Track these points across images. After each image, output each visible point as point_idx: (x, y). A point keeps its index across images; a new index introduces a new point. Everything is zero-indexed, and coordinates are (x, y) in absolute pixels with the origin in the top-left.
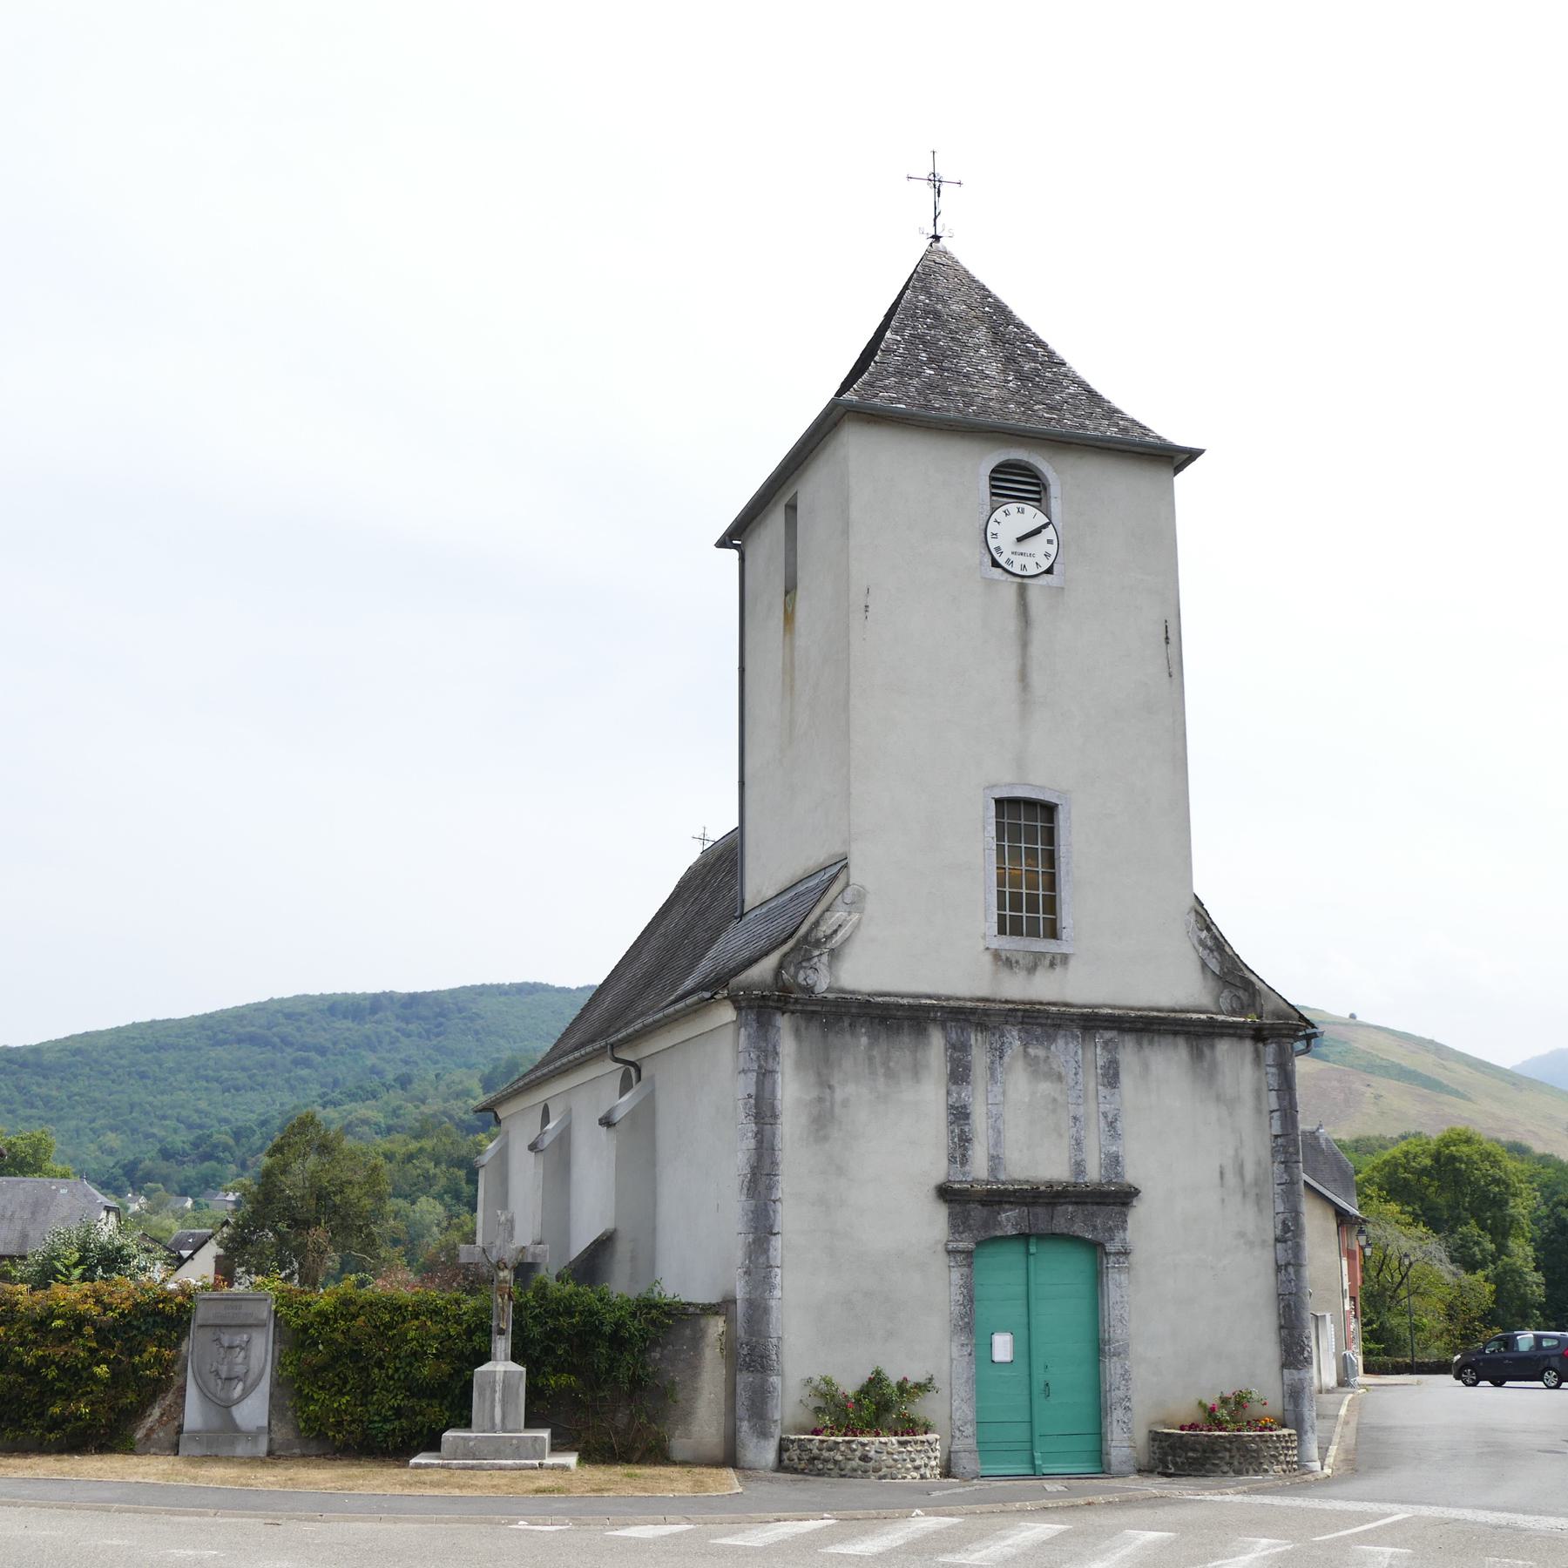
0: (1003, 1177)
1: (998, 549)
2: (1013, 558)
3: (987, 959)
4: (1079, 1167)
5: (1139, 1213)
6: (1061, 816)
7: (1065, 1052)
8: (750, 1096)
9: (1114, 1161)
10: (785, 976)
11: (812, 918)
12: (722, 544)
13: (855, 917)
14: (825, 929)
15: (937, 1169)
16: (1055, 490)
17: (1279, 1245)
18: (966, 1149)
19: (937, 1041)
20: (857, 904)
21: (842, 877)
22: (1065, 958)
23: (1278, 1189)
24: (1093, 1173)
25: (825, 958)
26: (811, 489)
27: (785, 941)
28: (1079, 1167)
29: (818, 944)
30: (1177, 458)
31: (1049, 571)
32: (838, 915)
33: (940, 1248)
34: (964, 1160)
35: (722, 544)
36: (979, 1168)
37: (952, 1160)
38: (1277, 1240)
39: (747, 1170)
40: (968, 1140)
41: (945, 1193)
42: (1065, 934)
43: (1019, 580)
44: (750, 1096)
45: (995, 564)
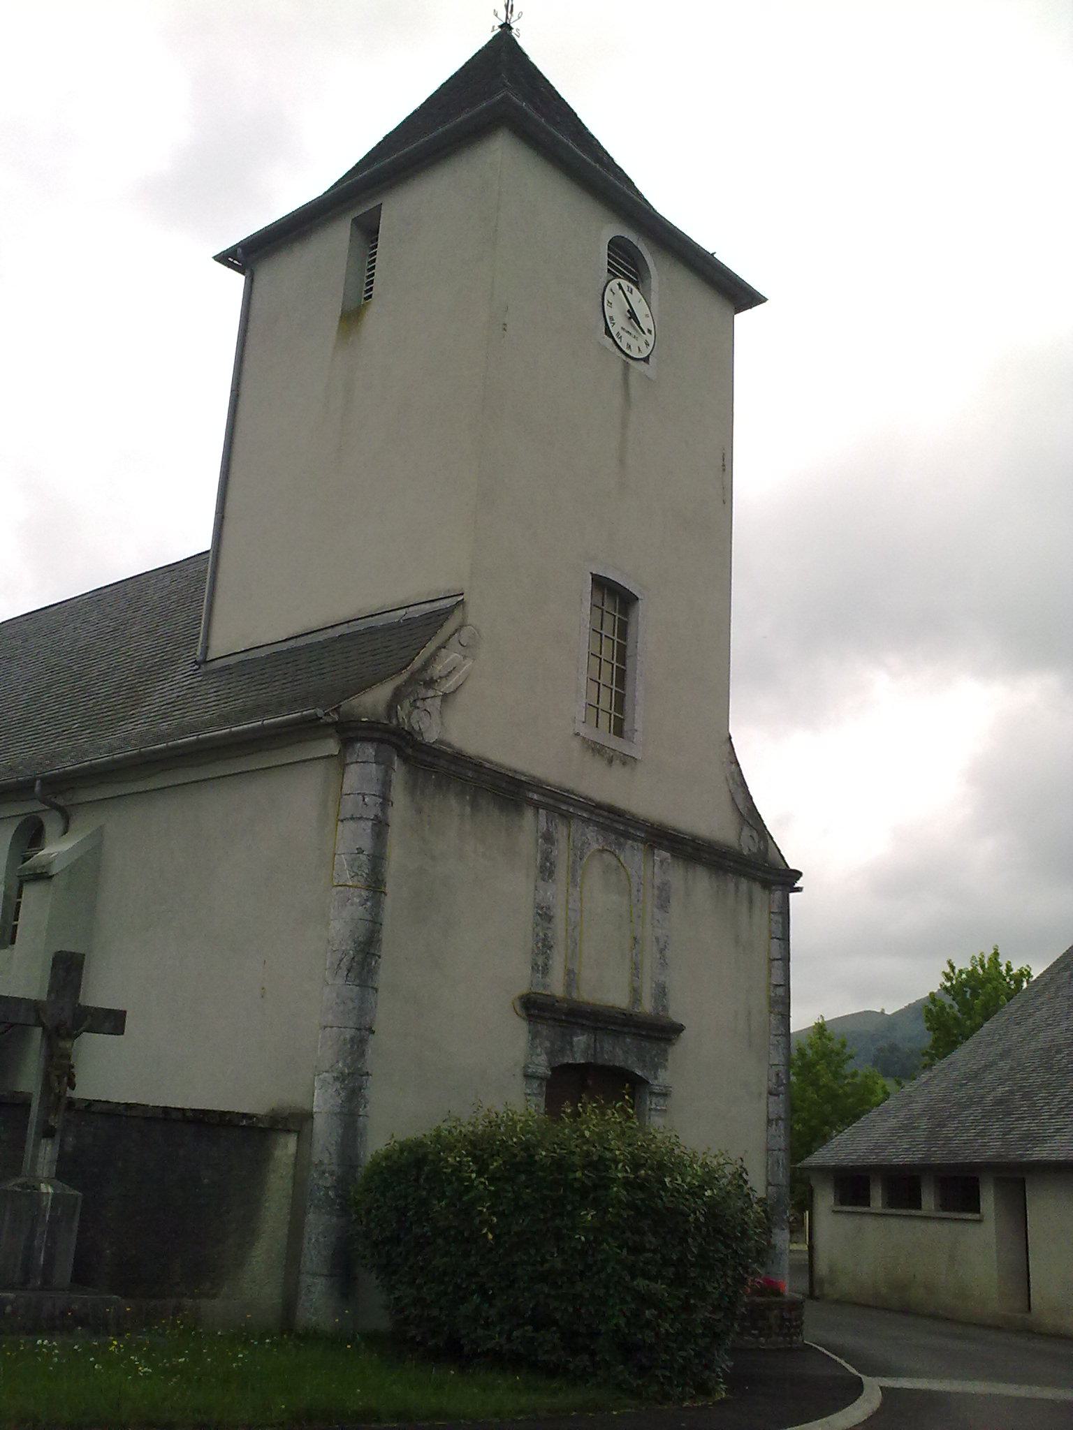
0: (575, 996)
1: (611, 318)
2: (622, 333)
3: (576, 744)
4: (636, 993)
5: (679, 1051)
6: (641, 606)
7: (633, 856)
8: (360, 851)
9: (661, 992)
10: (401, 714)
11: (425, 653)
12: (224, 258)
13: (469, 664)
14: (438, 669)
15: (521, 981)
16: (655, 282)
17: (772, 1098)
18: (547, 958)
19: (530, 824)
20: (468, 649)
21: (458, 613)
22: (627, 760)
23: (774, 1040)
24: (647, 1006)
25: (438, 701)
26: (396, 210)
27: (399, 672)
28: (636, 993)
29: (430, 683)
30: (742, 296)
31: (646, 360)
32: (451, 657)
33: (519, 1072)
34: (545, 970)
35: (224, 258)
36: (556, 986)
37: (535, 967)
38: (770, 1093)
39: (349, 946)
40: (550, 947)
41: (534, 1007)
42: (638, 737)
43: (624, 357)
44: (360, 851)
45: (608, 332)
